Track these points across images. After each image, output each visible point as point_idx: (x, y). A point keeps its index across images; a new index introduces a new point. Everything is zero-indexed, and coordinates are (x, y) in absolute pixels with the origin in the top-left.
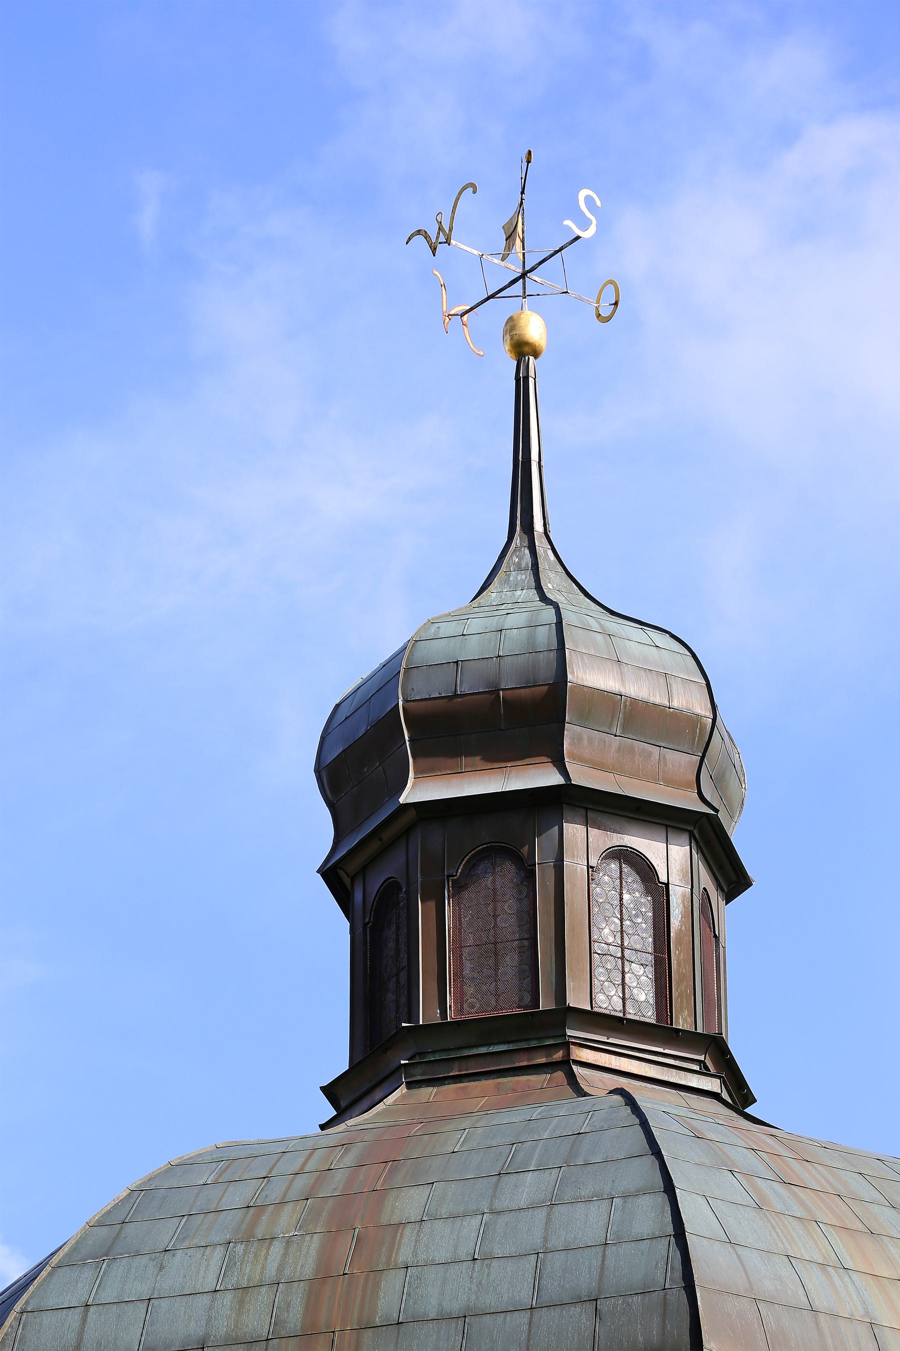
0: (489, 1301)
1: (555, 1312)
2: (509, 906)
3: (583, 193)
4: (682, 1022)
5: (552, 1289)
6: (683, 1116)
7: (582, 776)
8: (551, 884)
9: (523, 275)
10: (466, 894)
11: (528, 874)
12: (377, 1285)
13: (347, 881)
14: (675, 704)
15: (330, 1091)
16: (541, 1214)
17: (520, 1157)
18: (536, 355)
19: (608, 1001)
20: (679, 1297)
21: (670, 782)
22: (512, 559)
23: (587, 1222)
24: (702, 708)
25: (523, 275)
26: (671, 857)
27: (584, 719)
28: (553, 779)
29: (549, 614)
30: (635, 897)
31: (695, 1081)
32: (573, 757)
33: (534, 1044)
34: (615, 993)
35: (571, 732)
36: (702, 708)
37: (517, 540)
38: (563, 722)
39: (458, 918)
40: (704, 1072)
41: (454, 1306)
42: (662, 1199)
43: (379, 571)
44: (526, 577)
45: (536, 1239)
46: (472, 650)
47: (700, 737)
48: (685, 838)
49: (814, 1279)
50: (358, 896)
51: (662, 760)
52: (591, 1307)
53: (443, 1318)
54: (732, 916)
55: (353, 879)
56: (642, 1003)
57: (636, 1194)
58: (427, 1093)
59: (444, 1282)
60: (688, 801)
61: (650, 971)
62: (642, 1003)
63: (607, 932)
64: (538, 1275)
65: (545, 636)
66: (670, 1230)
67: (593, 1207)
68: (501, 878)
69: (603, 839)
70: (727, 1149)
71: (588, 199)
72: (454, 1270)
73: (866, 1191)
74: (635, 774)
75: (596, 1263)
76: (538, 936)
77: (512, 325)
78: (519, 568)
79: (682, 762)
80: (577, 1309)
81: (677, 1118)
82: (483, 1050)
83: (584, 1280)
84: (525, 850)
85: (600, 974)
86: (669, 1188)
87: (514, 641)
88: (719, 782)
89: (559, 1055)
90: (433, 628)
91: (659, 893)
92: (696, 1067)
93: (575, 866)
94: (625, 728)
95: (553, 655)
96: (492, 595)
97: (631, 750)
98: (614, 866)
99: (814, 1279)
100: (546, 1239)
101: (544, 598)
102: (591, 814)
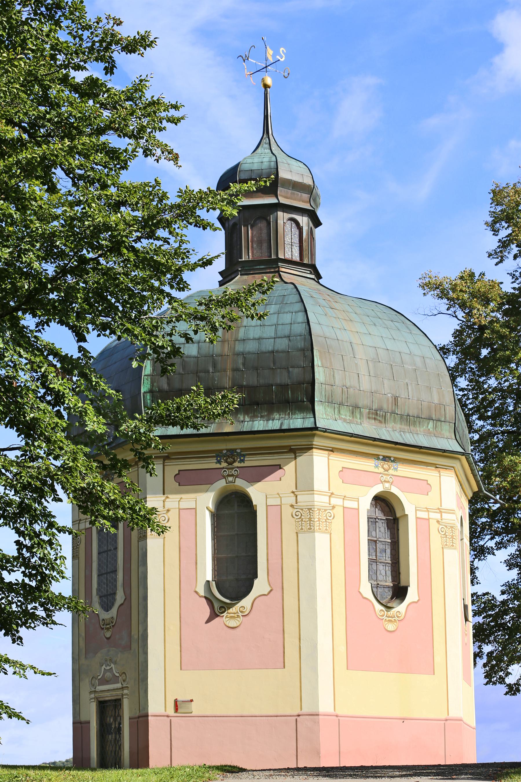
0: (265, 336)
1: (280, 339)
2: (265, 231)
3: (281, 49)
4: (305, 261)
5: (279, 334)
6: (306, 285)
7: (283, 201)
8: (275, 226)
9: (266, 67)
10: (254, 228)
11: (269, 223)
12: (239, 330)
13: (224, 221)
14: (305, 182)
15: (220, 273)
16: (276, 316)
17: (271, 300)
18: (269, 87)
19: (288, 256)
20: (308, 337)
21: (303, 201)
22: (264, 141)
23: (287, 318)
24: (311, 183)
25: (266, 67)
26: (304, 221)
27: (282, 187)
28: (275, 201)
29: (274, 159)
30: (296, 231)
31: (309, 276)
32: (280, 195)
33: (271, 266)
34: (290, 253)
35: (280, 189)
36: (311, 183)
37: (265, 136)
38: (277, 187)
39: (252, 234)
40: (311, 273)
41: (257, 336)
42: (304, 313)
43: (401, 608)
44: (267, 146)
45: (275, 322)
46: (255, 167)
47: (309, 190)
48: (307, 215)
49: (338, 332)
50: (227, 225)
51: (301, 196)
52: (288, 338)
53: (254, 339)
54: (318, 231)
55: (225, 220)
56: (296, 257)
57: (298, 312)
58: (245, 277)
59: (254, 330)
60: (307, 206)
61: (298, 248)
62: (296, 257)
63: (288, 240)
64: (276, 331)
65: (273, 164)
66: (306, 321)
67: (288, 314)
68: (262, 225)
69: (287, 216)
70: (319, 300)
71: (283, 51)
72: (256, 328)
73: (350, 310)
74: (295, 200)
75: (289, 328)
76: (271, 240)
77: (263, 80)
78: (266, 143)
79: (306, 196)
80: (285, 339)
81: (307, 292)
82: (258, 267)
83: (287, 332)
84: (269, 218)
85: (286, 249)
86: (306, 311)
87: (265, 166)
88: (315, 200)
89: (277, 269)
90: (245, 161)
91: (300, 229)
92: (309, 272)
93: (280, 222)
94: (293, 188)
95: (275, 170)
96: (259, 150)
97: (294, 194)
98: (289, 222)
99: (338, 332)
100: (277, 322)
101: (272, 153)
102: (284, 209)
